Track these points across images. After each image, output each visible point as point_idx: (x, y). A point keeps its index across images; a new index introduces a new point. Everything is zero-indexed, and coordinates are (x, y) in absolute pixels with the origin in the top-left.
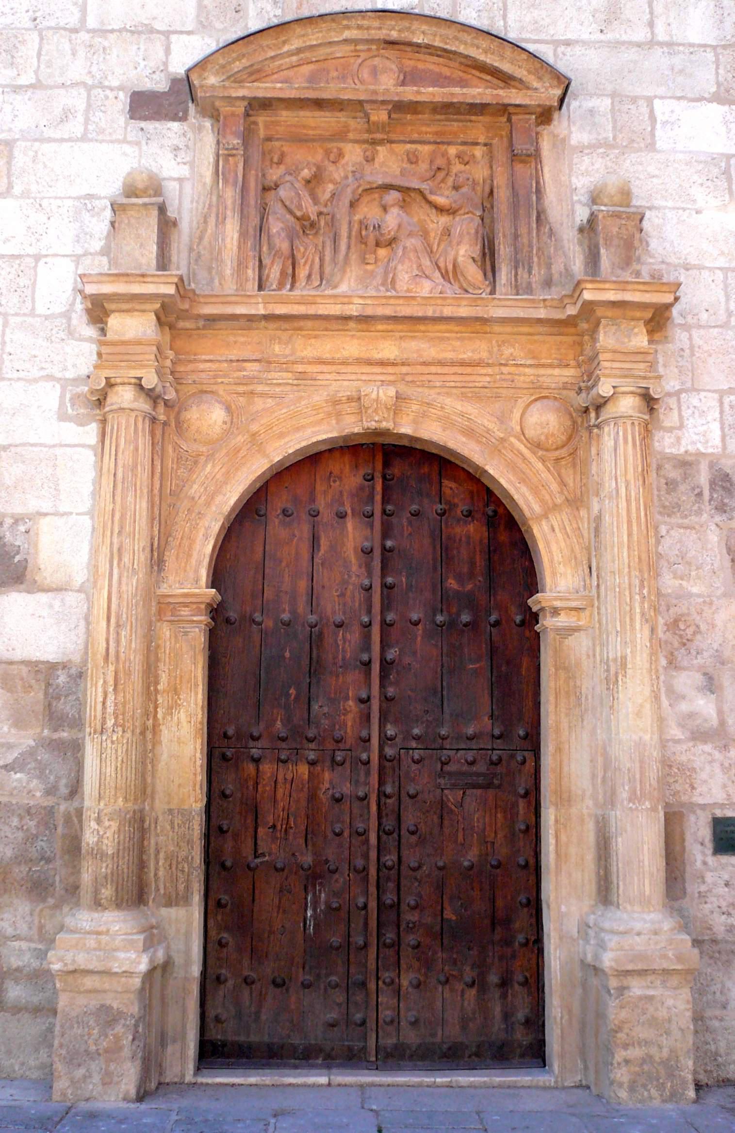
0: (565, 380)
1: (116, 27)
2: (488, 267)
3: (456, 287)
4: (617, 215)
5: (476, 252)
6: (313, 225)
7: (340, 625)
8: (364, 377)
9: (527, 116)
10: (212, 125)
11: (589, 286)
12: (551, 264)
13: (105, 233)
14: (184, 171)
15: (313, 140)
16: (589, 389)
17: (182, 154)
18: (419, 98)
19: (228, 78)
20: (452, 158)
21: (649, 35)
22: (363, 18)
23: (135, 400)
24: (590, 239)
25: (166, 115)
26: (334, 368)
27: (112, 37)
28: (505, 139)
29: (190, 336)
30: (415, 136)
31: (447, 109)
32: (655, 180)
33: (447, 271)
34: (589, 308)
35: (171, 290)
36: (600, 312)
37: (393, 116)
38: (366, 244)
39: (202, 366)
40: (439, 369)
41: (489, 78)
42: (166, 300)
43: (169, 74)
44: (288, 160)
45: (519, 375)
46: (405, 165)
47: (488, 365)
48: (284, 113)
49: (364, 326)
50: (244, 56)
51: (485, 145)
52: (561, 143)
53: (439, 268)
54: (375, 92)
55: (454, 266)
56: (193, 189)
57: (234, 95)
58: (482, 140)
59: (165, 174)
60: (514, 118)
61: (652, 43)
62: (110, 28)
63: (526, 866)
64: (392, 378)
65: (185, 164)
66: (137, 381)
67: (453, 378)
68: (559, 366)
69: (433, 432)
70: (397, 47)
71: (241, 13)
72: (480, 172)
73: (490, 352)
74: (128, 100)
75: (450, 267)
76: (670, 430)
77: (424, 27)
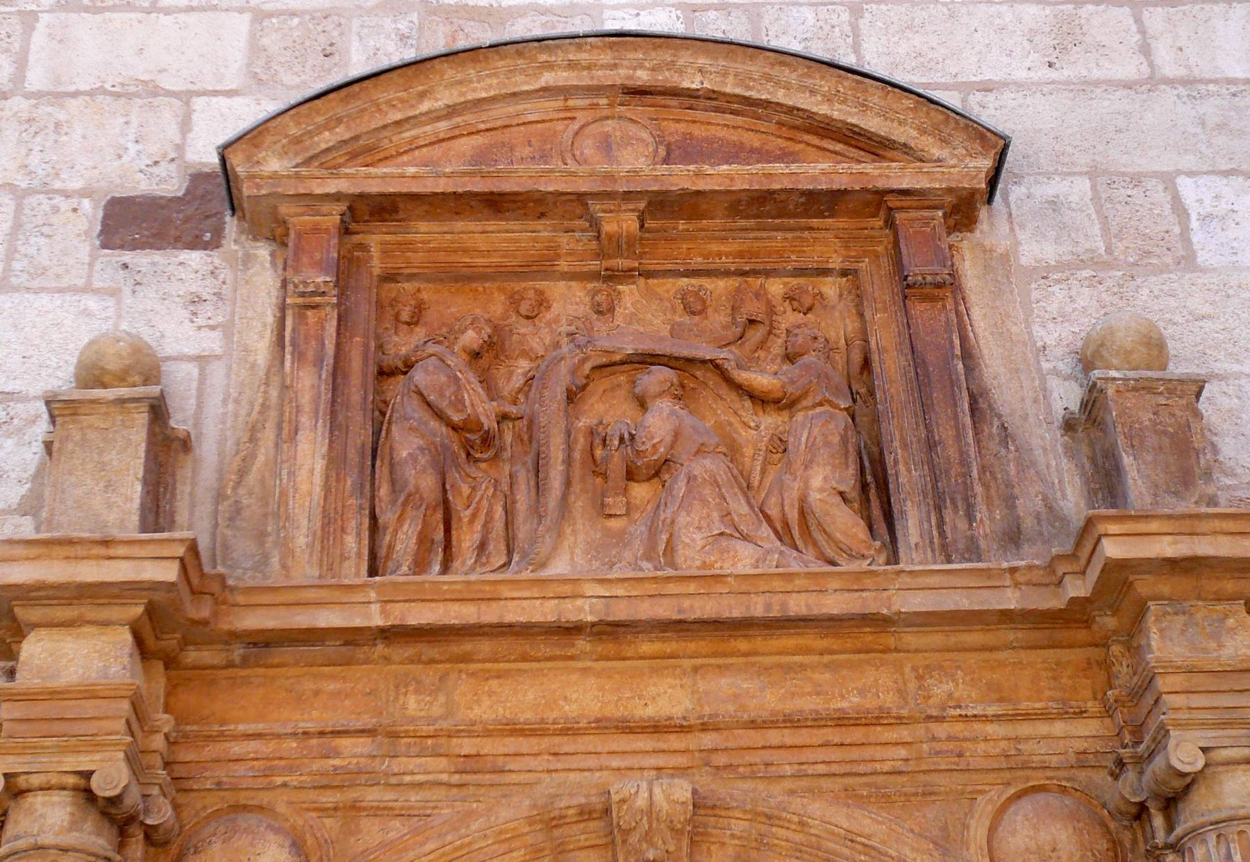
0: (1081, 745)
1: (84, 87)
2: (876, 512)
3: (810, 555)
4: (1144, 387)
5: (849, 483)
6: (487, 440)
8: (616, 762)
9: (926, 213)
10: (272, 255)
11: (1113, 528)
12: (1014, 498)
13: (32, 470)
14: (212, 342)
15: (484, 277)
16: (1142, 761)
17: (207, 310)
18: (702, 185)
19: (307, 162)
20: (777, 301)
21: (1145, 69)
22: (579, 48)
23: (74, 825)
24: (1091, 444)
25: (177, 239)
26: (545, 742)
27: (73, 103)
28: (884, 261)
29: (213, 682)
30: (697, 262)
31: (761, 205)
32: (1207, 324)
33: (786, 524)
34: (1119, 575)
35: (169, 573)
36: (1144, 585)
37: (650, 224)
38: (604, 476)
39: (237, 749)
40: (788, 737)
41: (839, 147)
42: (158, 596)
43: (188, 166)
44: (431, 316)
45: (975, 740)
46: (677, 319)
47: (900, 721)
48: (423, 226)
49: (610, 648)
50: (339, 121)
51: (844, 273)
52: (1001, 264)
53: (768, 519)
54: (609, 177)
55: (802, 513)
56: (228, 376)
57: (318, 191)
58: (836, 263)
59: (169, 348)
60: (899, 217)
61: (1153, 82)
62: (72, 89)
64: (681, 761)
65: (213, 328)
66: (82, 782)
67: (821, 755)
68: (1062, 715)
70: (649, 99)
71: (336, 58)
72: (838, 325)
73: (902, 693)
74: (100, 214)
75: (793, 516)
77: (702, 61)
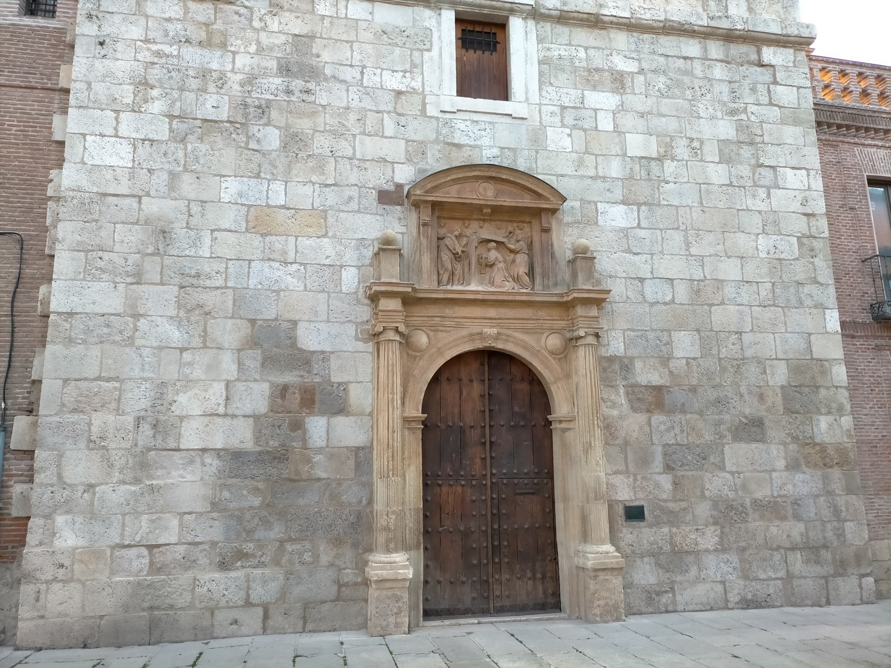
5: (527, 271)
7: (472, 427)
14: (403, 230)
17: (403, 221)
43: (394, 183)
63: (550, 528)
69: (510, 347)
76: (604, 346)
